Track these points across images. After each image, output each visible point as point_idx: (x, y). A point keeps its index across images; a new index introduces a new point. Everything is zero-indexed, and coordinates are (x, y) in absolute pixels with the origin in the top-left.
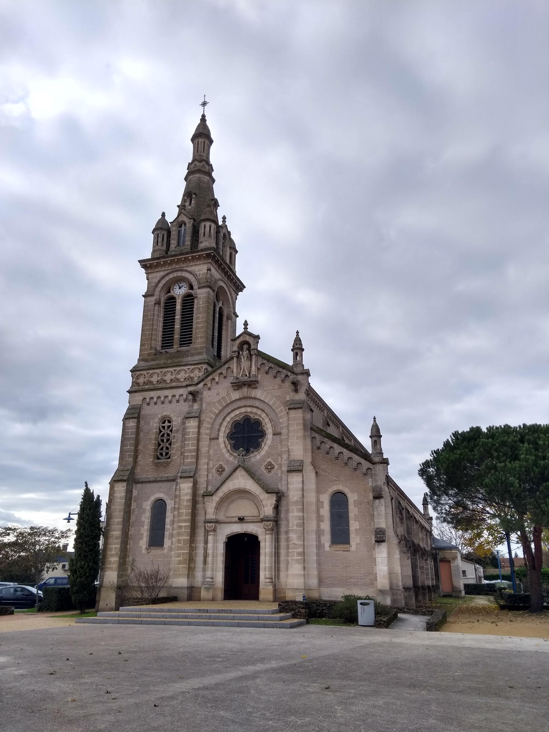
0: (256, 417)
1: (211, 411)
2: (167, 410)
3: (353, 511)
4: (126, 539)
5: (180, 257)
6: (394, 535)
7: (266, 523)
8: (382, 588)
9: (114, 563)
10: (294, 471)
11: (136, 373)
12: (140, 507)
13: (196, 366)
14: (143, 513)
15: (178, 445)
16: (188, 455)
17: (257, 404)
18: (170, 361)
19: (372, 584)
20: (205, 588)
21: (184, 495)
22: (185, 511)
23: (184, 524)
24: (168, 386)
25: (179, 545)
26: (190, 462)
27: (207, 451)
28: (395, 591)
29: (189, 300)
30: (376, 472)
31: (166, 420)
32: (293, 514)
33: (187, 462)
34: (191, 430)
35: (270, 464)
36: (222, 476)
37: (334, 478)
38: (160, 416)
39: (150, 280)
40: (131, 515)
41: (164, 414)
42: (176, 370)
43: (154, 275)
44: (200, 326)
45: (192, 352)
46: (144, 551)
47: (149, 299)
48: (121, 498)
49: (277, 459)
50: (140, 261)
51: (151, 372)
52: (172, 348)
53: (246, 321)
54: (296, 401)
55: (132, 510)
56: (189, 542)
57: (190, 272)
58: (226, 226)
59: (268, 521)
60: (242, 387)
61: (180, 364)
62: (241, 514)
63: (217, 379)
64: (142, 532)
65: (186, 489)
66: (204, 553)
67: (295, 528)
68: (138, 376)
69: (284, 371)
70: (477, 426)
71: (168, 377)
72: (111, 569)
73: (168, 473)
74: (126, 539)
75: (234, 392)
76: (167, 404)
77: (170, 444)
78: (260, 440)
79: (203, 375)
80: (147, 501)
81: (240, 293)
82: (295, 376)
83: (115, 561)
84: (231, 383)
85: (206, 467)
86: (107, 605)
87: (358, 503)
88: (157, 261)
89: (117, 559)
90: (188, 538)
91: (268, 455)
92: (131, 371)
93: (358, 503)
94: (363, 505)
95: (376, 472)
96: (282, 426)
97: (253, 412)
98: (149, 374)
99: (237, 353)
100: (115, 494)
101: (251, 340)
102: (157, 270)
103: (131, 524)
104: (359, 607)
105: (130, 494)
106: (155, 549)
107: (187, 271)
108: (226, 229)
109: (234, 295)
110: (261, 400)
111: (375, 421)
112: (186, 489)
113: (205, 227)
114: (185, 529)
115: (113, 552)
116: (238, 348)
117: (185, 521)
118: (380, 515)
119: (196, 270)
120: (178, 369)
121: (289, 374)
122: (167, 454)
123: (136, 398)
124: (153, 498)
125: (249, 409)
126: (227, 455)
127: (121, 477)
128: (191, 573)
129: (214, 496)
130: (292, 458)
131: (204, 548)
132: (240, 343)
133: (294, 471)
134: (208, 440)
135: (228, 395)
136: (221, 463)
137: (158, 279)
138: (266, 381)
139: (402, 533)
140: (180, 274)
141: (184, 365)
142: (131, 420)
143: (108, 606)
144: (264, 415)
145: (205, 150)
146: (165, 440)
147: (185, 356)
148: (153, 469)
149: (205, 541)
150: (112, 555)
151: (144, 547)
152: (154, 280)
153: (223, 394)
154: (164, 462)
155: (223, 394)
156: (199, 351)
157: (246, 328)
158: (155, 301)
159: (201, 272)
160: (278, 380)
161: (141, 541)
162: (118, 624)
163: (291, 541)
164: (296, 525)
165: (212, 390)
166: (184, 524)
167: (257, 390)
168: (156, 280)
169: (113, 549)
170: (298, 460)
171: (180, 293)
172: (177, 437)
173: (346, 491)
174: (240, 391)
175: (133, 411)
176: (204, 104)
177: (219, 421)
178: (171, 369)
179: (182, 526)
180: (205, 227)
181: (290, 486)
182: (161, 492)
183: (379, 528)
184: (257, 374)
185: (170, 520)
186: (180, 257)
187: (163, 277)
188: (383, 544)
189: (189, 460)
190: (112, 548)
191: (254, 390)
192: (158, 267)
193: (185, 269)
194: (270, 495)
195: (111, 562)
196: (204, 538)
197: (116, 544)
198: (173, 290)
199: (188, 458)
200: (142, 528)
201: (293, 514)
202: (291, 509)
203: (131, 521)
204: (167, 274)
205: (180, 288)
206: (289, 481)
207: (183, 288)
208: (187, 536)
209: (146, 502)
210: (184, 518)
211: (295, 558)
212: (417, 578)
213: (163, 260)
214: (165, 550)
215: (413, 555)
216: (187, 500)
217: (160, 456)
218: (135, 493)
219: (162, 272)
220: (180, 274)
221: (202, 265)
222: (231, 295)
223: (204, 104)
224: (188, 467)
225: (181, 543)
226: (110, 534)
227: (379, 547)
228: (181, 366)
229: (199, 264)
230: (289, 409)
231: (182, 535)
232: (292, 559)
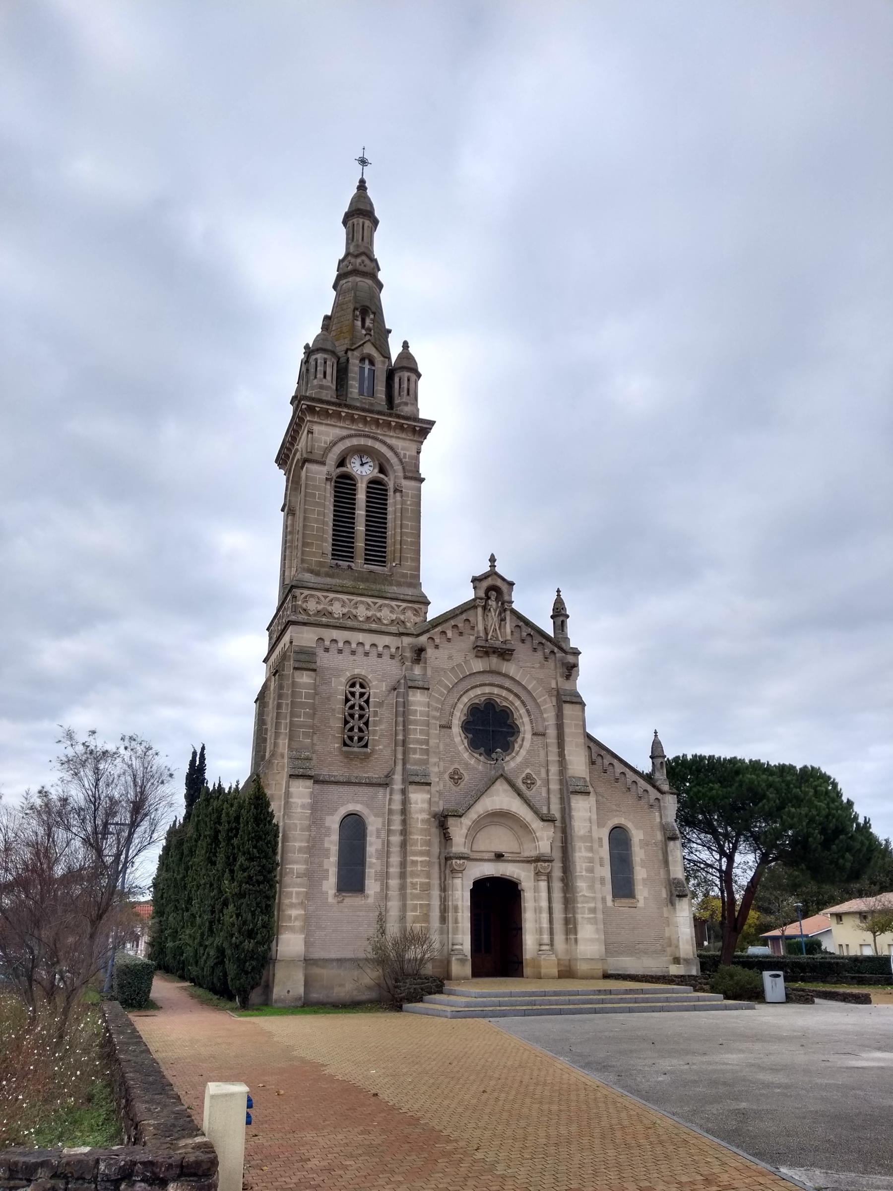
0: (505, 704)
1: (440, 682)
2: (361, 667)
3: (639, 854)
5: (376, 416)
9: (296, 918)
10: (579, 792)
11: (302, 591)
13: (410, 605)
14: (326, 835)
15: (383, 727)
17: (507, 683)
19: (664, 951)
20: (458, 959)
22: (420, 837)
23: (419, 859)
26: (420, 759)
32: (580, 854)
33: (414, 758)
34: (418, 708)
35: (528, 777)
36: (459, 787)
37: (615, 807)
38: (348, 674)
41: (356, 671)
42: (376, 603)
45: (399, 579)
46: (331, 900)
48: (303, 806)
49: (539, 771)
50: (435, 422)
51: (332, 595)
52: (385, 566)
53: (493, 556)
57: (391, 448)
61: (384, 595)
62: (501, 848)
63: (450, 634)
64: (325, 867)
65: (419, 801)
66: (440, 905)
67: (584, 873)
68: (306, 597)
69: (549, 643)
71: (362, 612)
72: (292, 929)
73: (366, 772)
75: (476, 660)
76: (359, 657)
80: (332, 815)
82: (564, 655)
86: (288, 992)
87: (644, 844)
88: (335, 408)
91: (526, 763)
93: (644, 844)
94: (650, 847)
96: (546, 723)
97: (501, 696)
98: (377, 605)
99: (484, 601)
100: (292, 797)
101: (504, 588)
102: (329, 422)
106: (350, 897)
107: (384, 443)
110: (474, 673)
111: (656, 736)
113: (409, 380)
114: (421, 866)
115: (294, 900)
120: (380, 602)
121: (556, 650)
122: (360, 739)
123: (305, 635)
124: (343, 811)
125: (496, 691)
126: (466, 755)
129: (463, 818)
131: (441, 897)
133: (579, 792)
136: (456, 766)
138: (522, 652)
140: (369, 442)
142: (305, 673)
143: (290, 993)
144: (518, 703)
147: (387, 583)
148: (341, 762)
149: (441, 886)
150: (292, 906)
152: (323, 438)
153: (459, 659)
155: (459, 659)
156: (409, 580)
157: (493, 566)
159: (408, 453)
160: (539, 655)
161: (325, 882)
162: (524, 1016)
163: (580, 892)
164: (586, 870)
165: (441, 650)
166: (419, 859)
167: (509, 664)
169: (294, 895)
171: (361, 472)
172: (382, 714)
173: (629, 825)
174: (486, 659)
177: (452, 700)
178: (369, 600)
179: (417, 861)
180: (409, 380)
182: (357, 802)
185: (377, 850)
186: (376, 416)
187: (343, 438)
188: (684, 899)
189: (417, 756)
191: (505, 663)
192: (331, 419)
193: (381, 437)
194: (546, 824)
196: (439, 882)
199: (415, 753)
200: (326, 861)
201: (580, 854)
202: (577, 847)
205: (362, 465)
207: (366, 467)
210: (420, 848)
211: (586, 916)
213: (347, 411)
214: (369, 899)
216: (423, 821)
217: (348, 742)
220: (369, 442)
221: (408, 442)
225: (417, 889)
226: (286, 868)
228: (386, 598)
229: (404, 439)
231: (418, 876)
232: (582, 918)
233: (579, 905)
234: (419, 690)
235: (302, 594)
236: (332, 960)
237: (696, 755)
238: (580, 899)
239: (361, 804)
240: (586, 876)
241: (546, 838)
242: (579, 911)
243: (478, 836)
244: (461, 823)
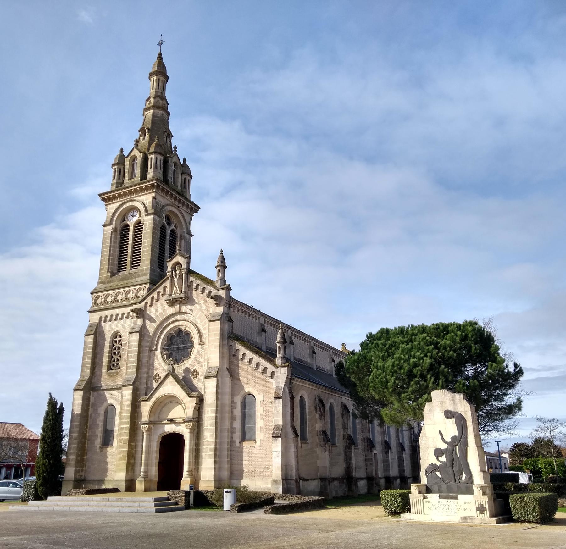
4: (83, 440)
6: (291, 431)
7: (188, 423)
8: (276, 479)
9: (72, 460)
11: (94, 295)
12: (95, 411)
16: (131, 366)
18: (122, 283)
21: (125, 401)
23: (124, 426)
24: (118, 306)
25: (121, 444)
26: (132, 371)
27: (147, 362)
28: (289, 481)
29: (139, 225)
30: (279, 375)
31: (116, 335)
33: (129, 371)
38: (112, 332)
39: (108, 211)
40: (89, 419)
42: (125, 290)
43: (111, 206)
44: (146, 249)
46: (98, 450)
47: (107, 228)
52: (126, 270)
54: (216, 314)
55: (89, 415)
56: (128, 442)
58: (177, 154)
59: (188, 421)
60: (175, 303)
64: (97, 434)
65: (127, 395)
70: (388, 327)
74: (83, 440)
77: (120, 356)
78: (190, 350)
79: (145, 294)
81: (195, 214)
83: (74, 458)
84: (165, 300)
85: (145, 375)
88: (112, 194)
89: (75, 457)
90: (128, 438)
92: (92, 293)
95: (279, 375)
103: (88, 426)
104: (225, 494)
105: (87, 400)
108: (177, 157)
109: (187, 217)
112: (127, 395)
114: (125, 430)
116: (172, 268)
117: (125, 423)
118: (279, 413)
119: (144, 199)
123: (95, 317)
127: (79, 387)
128: (130, 468)
130: (210, 365)
132: (174, 264)
133: (210, 377)
134: (148, 352)
135: (165, 310)
137: (114, 209)
139: (321, 429)
141: (131, 286)
145: (160, 87)
146: (116, 353)
151: (98, 446)
152: (148, 201)
153: (161, 310)
154: (114, 372)
158: (112, 229)
163: (206, 439)
164: (210, 425)
166: (124, 426)
168: (113, 211)
170: (215, 367)
175: (91, 328)
176: (161, 43)
179: (123, 428)
181: (207, 391)
183: (277, 425)
184: (187, 291)
187: (118, 208)
190: (71, 447)
195: (70, 459)
197: (74, 444)
198: (127, 218)
199: (130, 369)
202: (206, 411)
203: (88, 424)
204: (121, 205)
206: (206, 386)
208: (127, 436)
209: (100, 408)
210: (125, 420)
211: (208, 453)
212: (351, 469)
213: (117, 192)
215: (348, 448)
216: (128, 405)
218: (92, 399)
219: (117, 203)
222: (183, 217)
223: (161, 43)
224: (130, 376)
227: (275, 442)
230: (210, 321)
232: (206, 454)
233: (204, 447)
234: (134, 334)
235: (94, 296)
236: (96, 480)
237: (383, 329)
238: (205, 443)
239: (113, 399)
240: (210, 429)
241: (190, 408)
242: (204, 450)
243: (163, 410)
244: (147, 404)
